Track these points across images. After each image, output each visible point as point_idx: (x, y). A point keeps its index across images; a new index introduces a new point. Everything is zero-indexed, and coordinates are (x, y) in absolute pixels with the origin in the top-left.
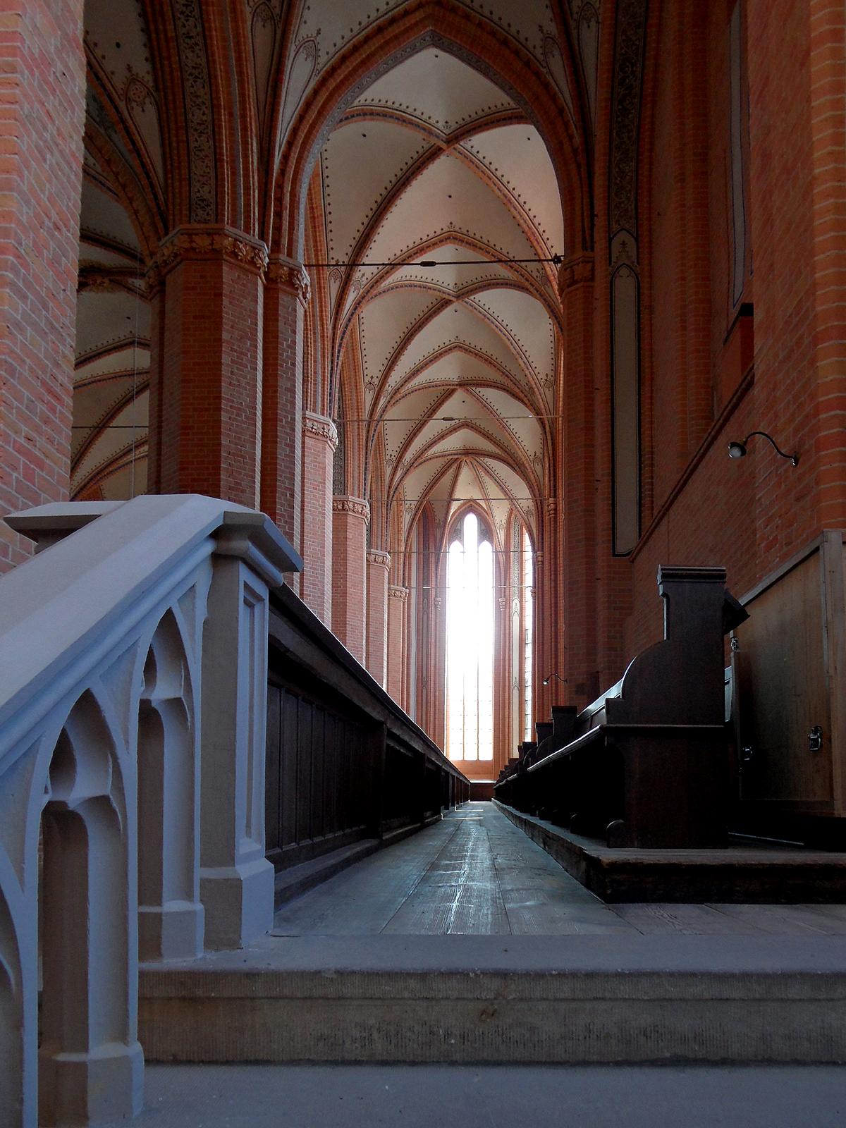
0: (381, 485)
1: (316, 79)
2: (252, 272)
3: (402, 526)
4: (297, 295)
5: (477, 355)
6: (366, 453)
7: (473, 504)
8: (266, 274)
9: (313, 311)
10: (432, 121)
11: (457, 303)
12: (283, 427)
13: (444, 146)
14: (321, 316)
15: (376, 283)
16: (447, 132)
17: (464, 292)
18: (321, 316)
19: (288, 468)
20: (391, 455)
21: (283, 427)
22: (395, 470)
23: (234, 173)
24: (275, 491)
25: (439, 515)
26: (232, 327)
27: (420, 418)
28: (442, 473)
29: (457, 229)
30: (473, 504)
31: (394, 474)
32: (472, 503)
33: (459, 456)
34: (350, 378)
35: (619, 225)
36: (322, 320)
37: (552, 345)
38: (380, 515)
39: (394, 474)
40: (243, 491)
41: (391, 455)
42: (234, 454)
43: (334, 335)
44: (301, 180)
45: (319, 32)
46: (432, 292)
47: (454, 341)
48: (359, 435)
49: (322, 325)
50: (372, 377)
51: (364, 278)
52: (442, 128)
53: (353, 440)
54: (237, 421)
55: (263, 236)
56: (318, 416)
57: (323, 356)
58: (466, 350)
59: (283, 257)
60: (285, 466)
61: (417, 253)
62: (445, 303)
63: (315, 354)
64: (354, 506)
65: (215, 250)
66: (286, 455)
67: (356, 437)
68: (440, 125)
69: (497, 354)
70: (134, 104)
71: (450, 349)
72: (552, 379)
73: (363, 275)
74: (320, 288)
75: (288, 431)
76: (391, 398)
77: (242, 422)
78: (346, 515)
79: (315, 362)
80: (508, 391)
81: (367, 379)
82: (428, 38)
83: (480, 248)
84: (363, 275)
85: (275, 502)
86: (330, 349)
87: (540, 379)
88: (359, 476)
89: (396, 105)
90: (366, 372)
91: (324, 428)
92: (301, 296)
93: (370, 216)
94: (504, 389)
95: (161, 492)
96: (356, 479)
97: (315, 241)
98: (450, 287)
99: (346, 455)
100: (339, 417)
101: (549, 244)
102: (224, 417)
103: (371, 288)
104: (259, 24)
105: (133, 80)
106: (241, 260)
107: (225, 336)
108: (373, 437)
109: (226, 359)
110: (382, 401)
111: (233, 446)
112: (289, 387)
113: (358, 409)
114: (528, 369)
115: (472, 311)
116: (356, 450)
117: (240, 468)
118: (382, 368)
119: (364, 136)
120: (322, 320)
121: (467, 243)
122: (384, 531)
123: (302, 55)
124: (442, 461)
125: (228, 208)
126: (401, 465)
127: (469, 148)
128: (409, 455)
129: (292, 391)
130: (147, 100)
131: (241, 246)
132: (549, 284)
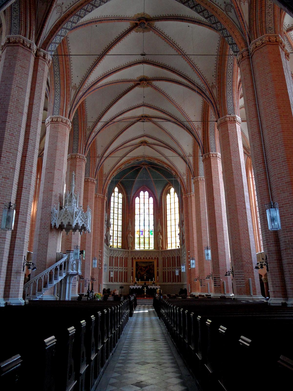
68: (286, 26)
106: (272, 42)
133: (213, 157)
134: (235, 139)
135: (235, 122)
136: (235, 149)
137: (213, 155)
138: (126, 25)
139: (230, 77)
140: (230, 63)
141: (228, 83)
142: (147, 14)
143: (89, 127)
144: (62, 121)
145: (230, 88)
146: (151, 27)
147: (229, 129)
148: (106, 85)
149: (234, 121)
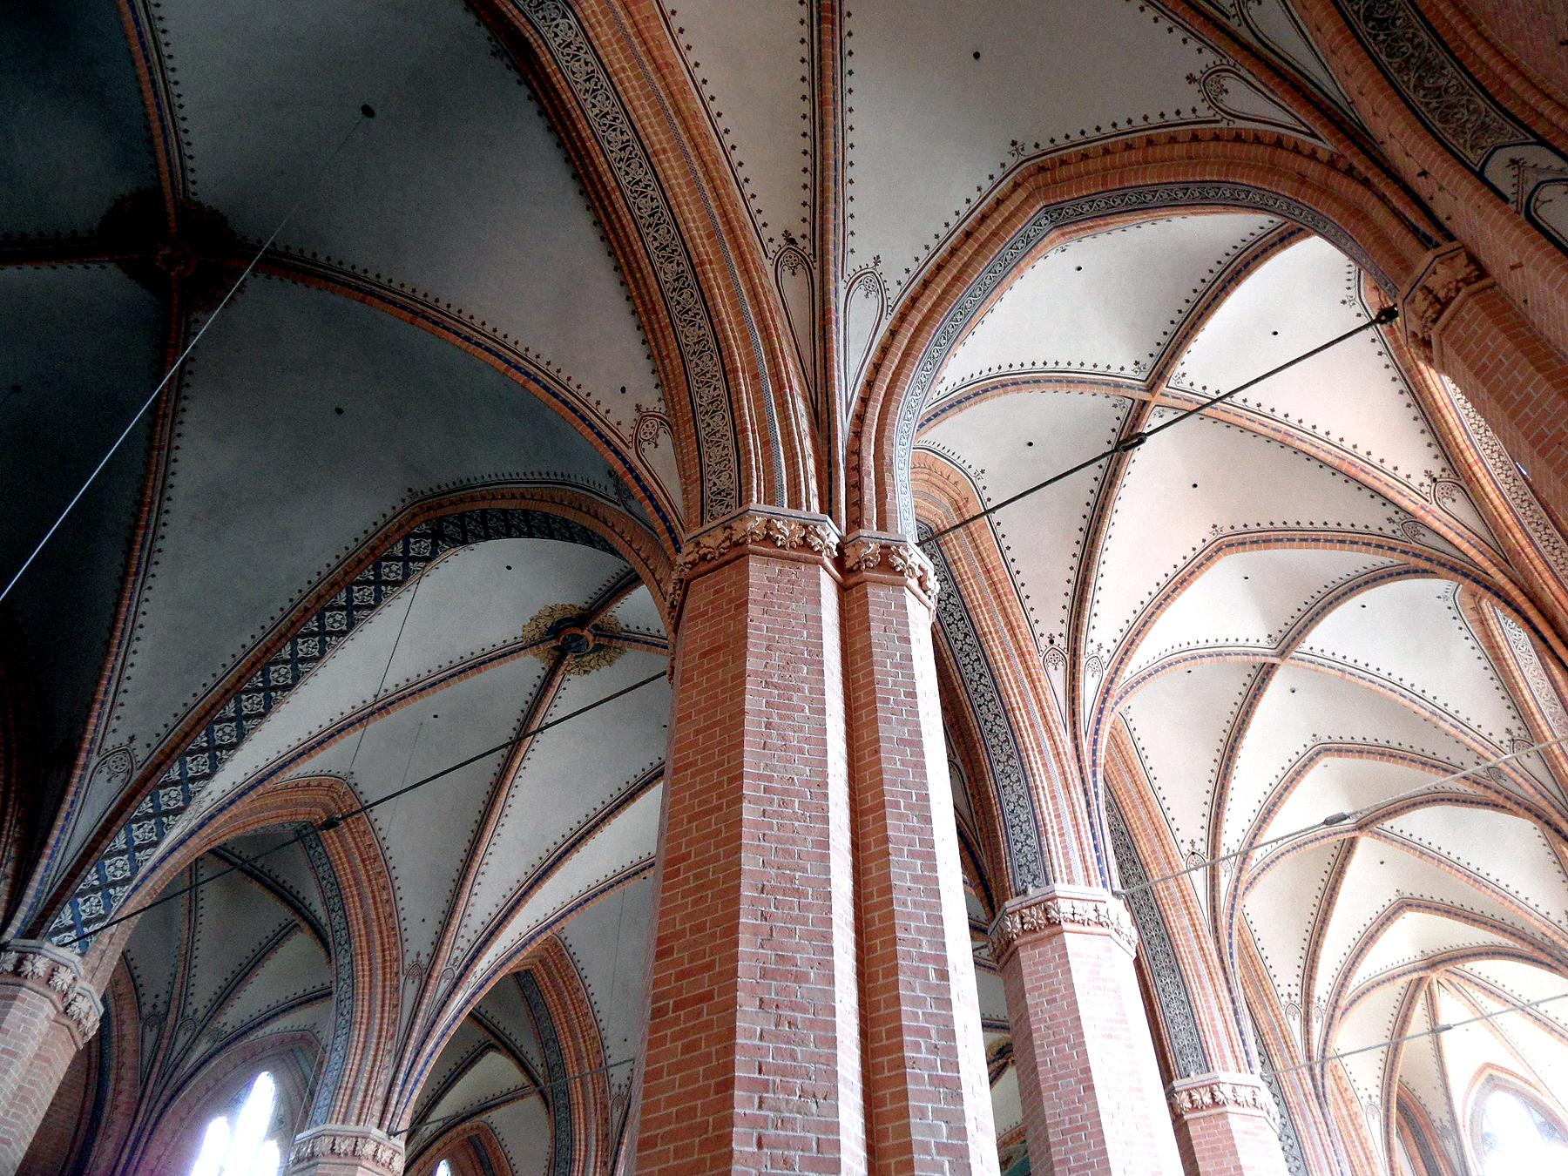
0: (1292, 1058)
1: (890, 318)
2: (806, 562)
3: (1370, 1145)
4: (904, 584)
5: (1364, 750)
6: (1227, 979)
7: (1495, 1073)
8: (839, 562)
9: (1029, 719)
10: (1115, 370)
11: (1283, 664)
12: (901, 817)
13: (1146, 396)
14: (1047, 723)
15: (1126, 653)
16: (1143, 376)
17: (1289, 640)
18: (1047, 723)
19: (924, 906)
20: (1289, 995)
21: (901, 817)
22: (1307, 1020)
23: (767, 443)
24: (894, 971)
25: (1437, 1112)
26: (768, 648)
27: (1387, 1041)
28: (1403, 1020)
29: (1227, 531)
30: (1495, 1073)
31: (1307, 1031)
32: (1490, 1071)
33: (1422, 974)
34: (1154, 852)
35: (1482, 148)
36: (1049, 730)
37: (1490, 673)
38: (1310, 1119)
39: (1307, 1031)
40: (800, 978)
41: (1289, 995)
42: (774, 890)
43: (1077, 750)
44: (891, 438)
45: (877, 260)
46: (1233, 658)
47: (1312, 744)
48: (1202, 949)
49: (1052, 737)
50: (1193, 843)
51: (1103, 652)
52: (1132, 375)
53: (1193, 958)
54: (781, 816)
55: (828, 506)
56: (1080, 889)
57: (1067, 786)
58: (1339, 751)
59: (870, 530)
60: (915, 904)
61: (1176, 588)
62: (1265, 673)
63: (1051, 785)
64: (1234, 1091)
65: (737, 544)
66: (915, 879)
67: (1197, 954)
68: (1128, 372)
69: (1393, 735)
70: (645, 445)
71: (1311, 759)
72: (1523, 733)
73: (1100, 647)
74: (1033, 681)
75: (915, 823)
76: (1241, 870)
77: (795, 815)
78: (1223, 1115)
79: (1053, 798)
80: (1450, 800)
81: (1186, 847)
82: (1043, 221)
83: (1277, 540)
84: (1100, 647)
85: (898, 998)
86: (1076, 774)
87: (1498, 744)
88: (1227, 1027)
89: (1051, 366)
90: (1179, 836)
91: (1096, 910)
92: (913, 583)
93: (1079, 554)
94: (1442, 800)
95: (511, 981)
96: (1223, 1035)
97: (1006, 616)
98: (1263, 643)
99: (1189, 992)
100: (1125, 882)
101: (1388, 467)
102: (749, 813)
103: (1120, 663)
104: (786, 274)
105: (642, 415)
106: (783, 547)
107: (752, 664)
108: (1231, 947)
109: (752, 702)
110: (1225, 883)
111: (773, 872)
112: (906, 736)
113: (1186, 902)
114: (1465, 734)
115: (1316, 671)
116: (1206, 978)
117: (793, 920)
118: (1205, 822)
119: (1030, 444)
120: (1049, 730)
121: (1252, 542)
122: (1331, 1154)
123: (858, 293)
124: (1393, 991)
125: (758, 485)
126: (1314, 1011)
127: (1188, 388)
128: (1323, 987)
129: (916, 744)
130: (661, 432)
131: (779, 524)
132: (1423, 530)
133: (1195, 1108)
134: (1067, 1040)
135: (1055, 929)
136: (1076, 1110)
137: (1190, 1096)
138: (530, 667)
139: (988, 697)
140: (961, 637)
141: (989, 725)
142: (564, 608)
143: (620, 1087)
144: (332, 1150)
145: (1005, 746)
146: (613, 636)
147: (1027, 987)
148: (586, 901)
149: (1051, 923)
